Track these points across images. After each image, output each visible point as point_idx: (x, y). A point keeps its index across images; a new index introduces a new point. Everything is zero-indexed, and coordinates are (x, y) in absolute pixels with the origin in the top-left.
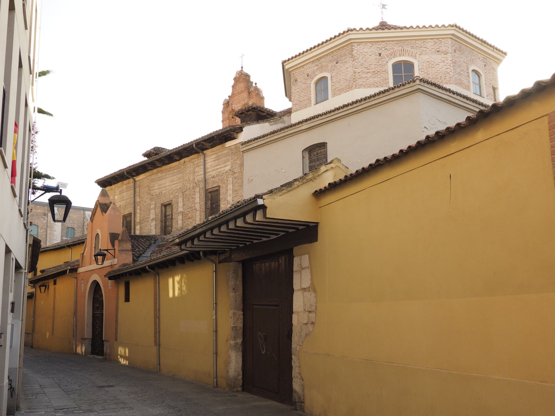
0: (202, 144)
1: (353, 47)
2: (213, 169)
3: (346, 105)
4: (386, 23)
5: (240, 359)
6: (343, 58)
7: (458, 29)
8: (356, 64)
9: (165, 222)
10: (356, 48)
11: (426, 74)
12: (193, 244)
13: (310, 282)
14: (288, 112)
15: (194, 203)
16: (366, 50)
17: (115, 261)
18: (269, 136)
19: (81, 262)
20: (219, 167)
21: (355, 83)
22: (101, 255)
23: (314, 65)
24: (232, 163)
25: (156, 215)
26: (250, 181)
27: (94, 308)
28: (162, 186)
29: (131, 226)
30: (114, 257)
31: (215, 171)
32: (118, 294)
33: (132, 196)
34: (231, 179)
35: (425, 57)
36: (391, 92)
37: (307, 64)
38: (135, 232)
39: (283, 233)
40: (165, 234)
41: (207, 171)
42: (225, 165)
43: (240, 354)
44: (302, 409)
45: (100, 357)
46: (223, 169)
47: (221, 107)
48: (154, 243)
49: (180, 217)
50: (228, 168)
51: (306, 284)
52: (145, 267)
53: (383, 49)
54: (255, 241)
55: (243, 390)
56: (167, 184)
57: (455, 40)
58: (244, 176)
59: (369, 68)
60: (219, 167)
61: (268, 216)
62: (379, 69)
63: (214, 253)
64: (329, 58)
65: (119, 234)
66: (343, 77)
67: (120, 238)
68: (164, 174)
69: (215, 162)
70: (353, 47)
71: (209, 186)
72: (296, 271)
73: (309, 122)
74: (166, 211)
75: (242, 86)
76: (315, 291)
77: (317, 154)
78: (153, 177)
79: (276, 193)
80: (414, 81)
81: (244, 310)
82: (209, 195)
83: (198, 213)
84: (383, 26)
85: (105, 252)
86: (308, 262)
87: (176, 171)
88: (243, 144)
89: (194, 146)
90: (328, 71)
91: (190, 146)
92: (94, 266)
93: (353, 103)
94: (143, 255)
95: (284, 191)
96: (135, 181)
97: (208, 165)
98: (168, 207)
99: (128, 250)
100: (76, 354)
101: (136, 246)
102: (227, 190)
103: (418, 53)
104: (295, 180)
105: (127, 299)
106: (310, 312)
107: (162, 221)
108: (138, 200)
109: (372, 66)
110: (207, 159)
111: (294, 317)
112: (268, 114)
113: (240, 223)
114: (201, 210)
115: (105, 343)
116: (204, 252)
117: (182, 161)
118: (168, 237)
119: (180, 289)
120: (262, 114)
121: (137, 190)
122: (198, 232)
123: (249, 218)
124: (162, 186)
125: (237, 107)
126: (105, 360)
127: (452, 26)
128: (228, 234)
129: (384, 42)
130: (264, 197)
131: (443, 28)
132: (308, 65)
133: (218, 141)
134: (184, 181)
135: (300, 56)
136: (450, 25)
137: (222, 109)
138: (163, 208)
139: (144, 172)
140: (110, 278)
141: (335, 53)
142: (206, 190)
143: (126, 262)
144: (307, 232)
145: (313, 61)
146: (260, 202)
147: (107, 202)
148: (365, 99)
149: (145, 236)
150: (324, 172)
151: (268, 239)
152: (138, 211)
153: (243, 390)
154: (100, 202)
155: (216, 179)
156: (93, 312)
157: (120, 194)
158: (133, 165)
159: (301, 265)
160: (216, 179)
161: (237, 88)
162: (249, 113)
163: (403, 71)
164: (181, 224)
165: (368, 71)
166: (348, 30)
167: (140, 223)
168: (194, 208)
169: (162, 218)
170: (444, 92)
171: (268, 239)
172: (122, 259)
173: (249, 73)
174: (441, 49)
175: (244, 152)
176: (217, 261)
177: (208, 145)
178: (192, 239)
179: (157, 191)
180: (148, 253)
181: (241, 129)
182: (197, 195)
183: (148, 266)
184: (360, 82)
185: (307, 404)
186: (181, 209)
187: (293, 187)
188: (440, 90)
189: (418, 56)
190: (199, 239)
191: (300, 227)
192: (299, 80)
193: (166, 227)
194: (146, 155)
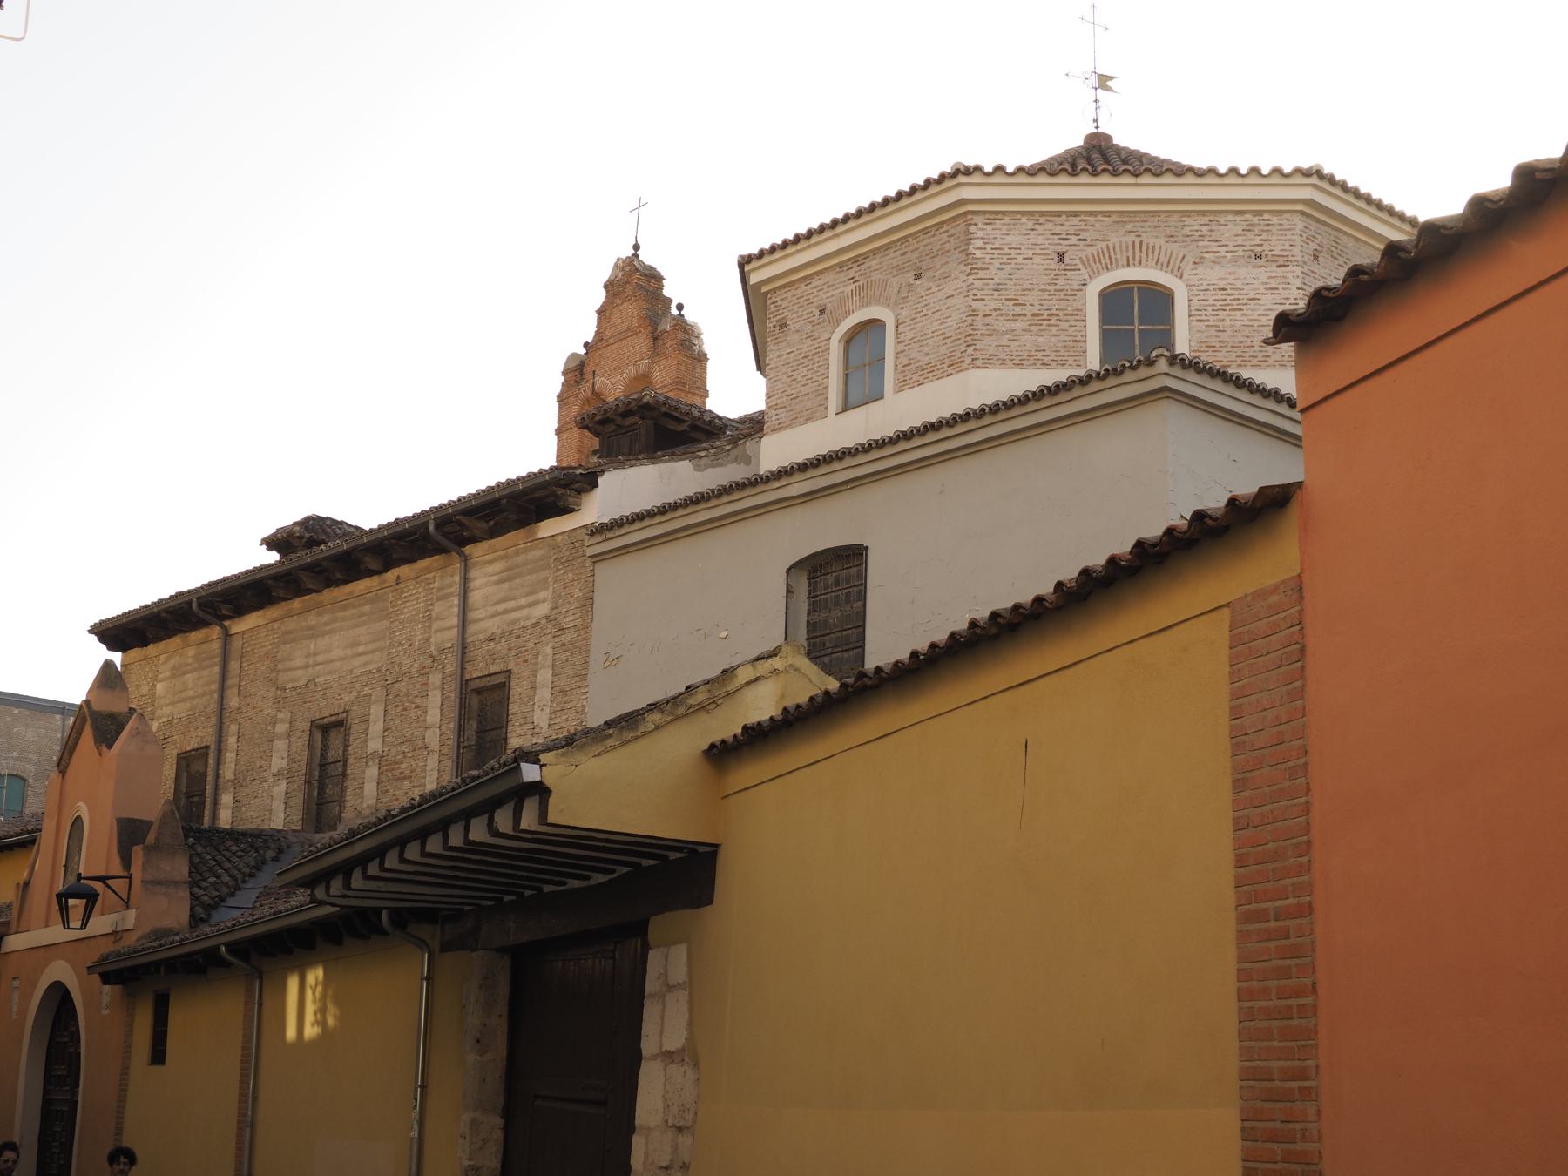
0: (460, 523)
1: (972, 229)
2: (491, 610)
3: (932, 425)
4: (1108, 138)
6: (938, 262)
7: (1325, 185)
8: (978, 284)
10: (981, 230)
11: (1213, 331)
12: (347, 886)
13: (685, 1034)
14: (754, 426)
16: (1014, 239)
18: (680, 512)
20: (511, 604)
21: (970, 350)
22: (80, 894)
23: (843, 277)
24: (557, 597)
25: (291, 760)
26: (612, 661)
28: (319, 659)
30: (127, 905)
31: (497, 619)
32: (129, 1034)
33: (214, 687)
34: (549, 650)
35: (1212, 274)
36: (1095, 386)
37: (821, 272)
38: (215, 816)
39: (625, 870)
40: (318, 830)
41: (472, 615)
42: (531, 599)
46: (525, 612)
47: (556, 383)
48: (276, 859)
49: (373, 771)
50: (542, 610)
51: (674, 1041)
52: (217, 947)
53: (1074, 240)
54: (547, 888)
56: (337, 653)
57: (1319, 221)
58: (593, 642)
59: (1021, 300)
60: (511, 604)
61: (551, 819)
62: (1054, 305)
63: (427, 915)
64: (894, 258)
65: (149, 824)
66: (936, 326)
68: (327, 617)
69: (499, 591)
70: (972, 229)
71: (476, 670)
72: (651, 995)
73: (812, 473)
74: (325, 747)
75: (631, 311)
76: (696, 1065)
77: (837, 583)
78: (290, 624)
79: (583, 746)
80: (1151, 363)
81: (508, 1113)
82: (475, 700)
83: (433, 761)
84: (1099, 156)
85: (98, 886)
86: (685, 968)
87: (367, 608)
88: (597, 530)
89: (431, 527)
91: (419, 526)
92: (56, 933)
93: (955, 420)
94: (231, 902)
95: (610, 742)
96: (227, 635)
97: (475, 597)
98: (333, 733)
99: (175, 883)
101: (211, 869)
102: (534, 689)
103: (1190, 259)
104: (653, 707)
106: (680, 1130)
107: (308, 783)
108: (233, 701)
109: (1033, 296)
110: (473, 574)
111: (638, 1142)
112: (694, 427)
113: (479, 832)
114: (445, 750)
116: (394, 912)
117: (391, 575)
119: (322, 1023)
120: (673, 426)
121: (234, 666)
122: (359, 848)
123: (503, 820)
124: (319, 659)
125: (613, 387)
127: (1306, 173)
128: (451, 864)
129: (1076, 214)
130: (543, 758)
131: (1276, 179)
132: (825, 278)
133: (512, 517)
134: (391, 645)
135: (800, 246)
136: (1298, 171)
137: (558, 388)
138: (318, 736)
139: (261, 607)
140: (106, 978)
142: (464, 683)
143: (167, 922)
144: (679, 875)
145: (841, 265)
146: (530, 773)
147: (119, 707)
148: (995, 409)
149: (244, 834)
150: (748, 683)
151: (585, 883)
152: (232, 740)
154: (95, 708)
155: (500, 647)
156: (46, 1092)
157: (173, 677)
158: (225, 580)
159: (666, 975)
160: (500, 647)
162: (630, 420)
163: (1137, 315)
164: (367, 795)
165: (1018, 310)
167: (237, 784)
168: (420, 742)
169: (309, 772)
170: (1256, 399)
171: (585, 883)
172: (152, 911)
174: (1266, 247)
175: (597, 558)
177: (480, 526)
178: (345, 869)
179: (301, 677)
180: (247, 896)
181: (589, 481)
182: (434, 698)
183: (226, 944)
184: (988, 345)
186: (375, 745)
187: (642, 729)
188: (1243, 395)
190: (364, 870)
191: (673, 856)
192: (792, 326)
193: (321, 803)
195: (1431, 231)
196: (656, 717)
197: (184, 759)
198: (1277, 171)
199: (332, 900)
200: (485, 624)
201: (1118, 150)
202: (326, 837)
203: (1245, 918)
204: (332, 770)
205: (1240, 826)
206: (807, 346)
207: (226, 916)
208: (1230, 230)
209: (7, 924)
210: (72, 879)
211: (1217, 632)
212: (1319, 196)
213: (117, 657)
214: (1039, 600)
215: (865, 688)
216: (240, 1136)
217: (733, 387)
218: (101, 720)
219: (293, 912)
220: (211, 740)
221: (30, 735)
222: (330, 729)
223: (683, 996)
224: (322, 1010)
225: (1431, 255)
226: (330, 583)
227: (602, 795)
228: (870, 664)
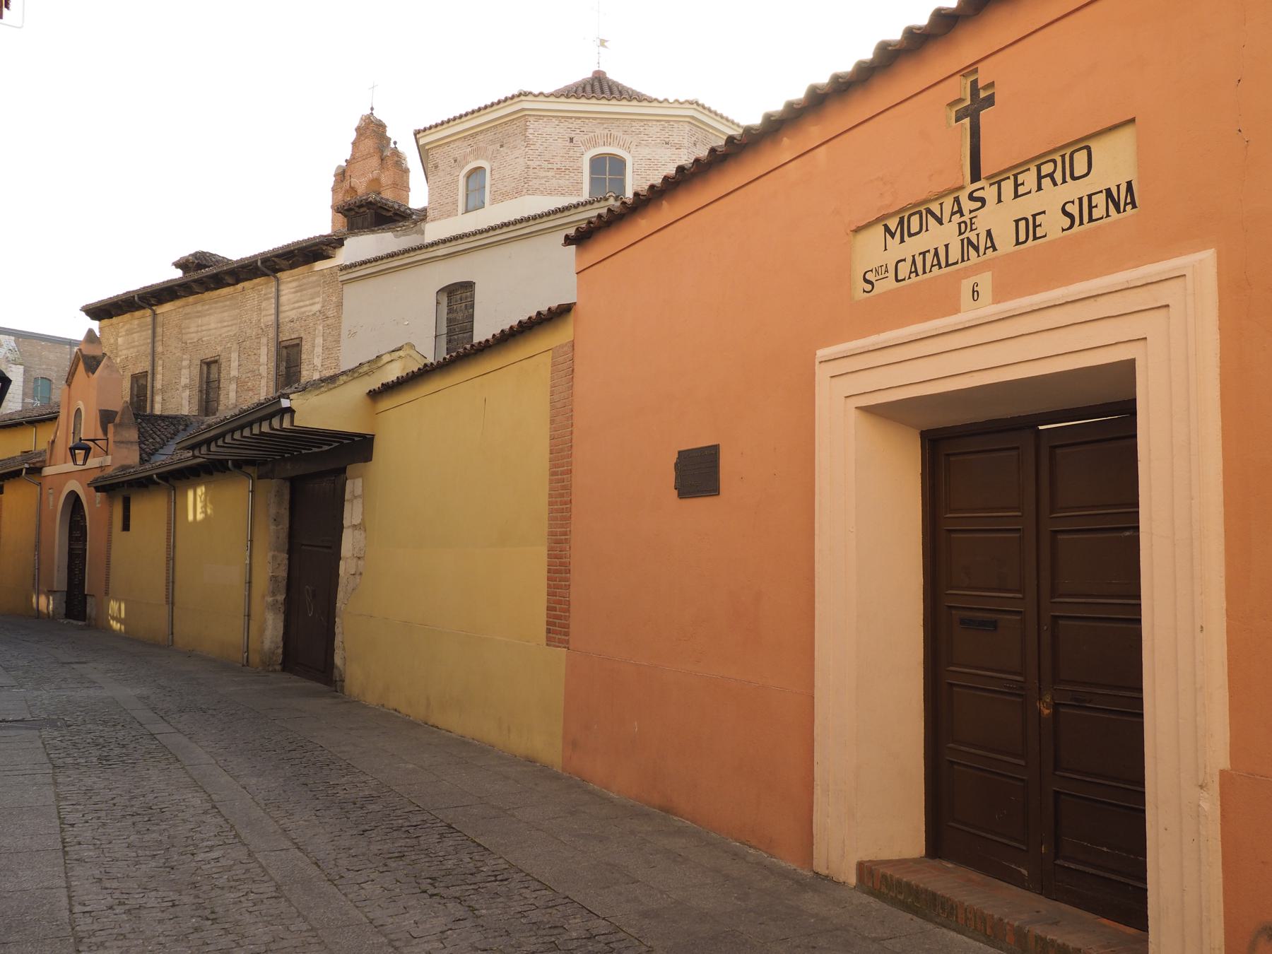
4: (604, 73)
5: (281, 625)
6: (511, 139)
9: (208, 394)
10: (532, 124)
12: (209, 450)
14: (423, 215)
15: (257, 362)
16: (549, 130)
17: (108, 460)
19: (48, 452)
22: (81, 448)
23: (466, 144)
25: (191, 380)
27: (71, 538)
29: (145, 396)
32: (111, 517)
34: (321, 328)
35: (645, 152)
40: (207, 415)
41: (282, 309)
43: (281, 617)
44: (342, 691)
45: (80, 623)
47: (331, 181)
49: (233, 386)
50: (317, 307)
51: (357, 521)
55: (283, 670)
56: (213, 326)
64: (490, 135)
67: (117, 420)
71: (284, 336)
73: (448, 244)
74: (208, 373)
75: (369, 144)
78: (188, 309)
80: (606, 200)
81: (290, 552)
82: (284, 352)
83: (264, 382)
84: (599, 86)
85: (91, 444)
90: (486, 159)
92: (70, 467)
93: (516, 222)
94: (161, 451)
96: (155, 314)
97: (283, 299)
100: (38, 614)
103: (634, 143)
104: (344, 373)
105: (126, 527)
107: (201, 391)
108: (159, 349)
109: (557, 159)
110: (282, 287)
112: (396, 214)
115: (89, 599)
117: (240, 286)
118: (211, 420)
119: (205, 512)
120: (384, 213)
121: (159, 330)
125: (361, 185)
126: (89, 626)
127: (691, 103)
137: (332, 184)
138: (205, 368)
139: (172, 300)
140: (98, 489)
141: (500, 129)
142: (279, 343)
143: (128, 462)
144: (357, 448)
145: (465, 137)
149: (168, 417)
152: (160, 369)
153: (283, 670)
155: (296, 325)
160: (296, 325)
161: (362, 147)
164: (232, 400)
166: (520, 95)
167: (163, 391)
169: (201, 386)
172: (120, 456)
173: (385, 121)
175: (344, 282)
176: (255, 476)
177: (284, 263)
178: (208, 442)
179: (195, 337)
180: (171, 447)
182: (264, 351)
185: (347, 682)
186: (234, 373)
189: (633, 148)
192: (441, 167)
194: (182, 265)
195: (748, 131)
196: (344, 378)
197: (135, 378)
198: (677, 101)
199: (202, 456)
200: (288, 313)
201: (608, 81)
202: (211, 420)
203: (553, 474)
204: (214, 385)
205: (552, 438)
206: (448, 178)
207: (159, 459)
208: (654, 129)
209: (44, 461)
210: (77, 440)
211: (547, 358)
212: (696, 114)
213: (95, 325)
214: (487, 341)
215: (427, 372)
216: (168, 564)
217: (418, 196)
218: (88, 359)
219: (187, 459)
220: (149, 369)
221: (52, 356)
222: (210, 364)
223: (360, 501)
224: (205, 506)
225: (740, 147)
226: (208, 289)
227: (315, 411)
228: (476, 340)
